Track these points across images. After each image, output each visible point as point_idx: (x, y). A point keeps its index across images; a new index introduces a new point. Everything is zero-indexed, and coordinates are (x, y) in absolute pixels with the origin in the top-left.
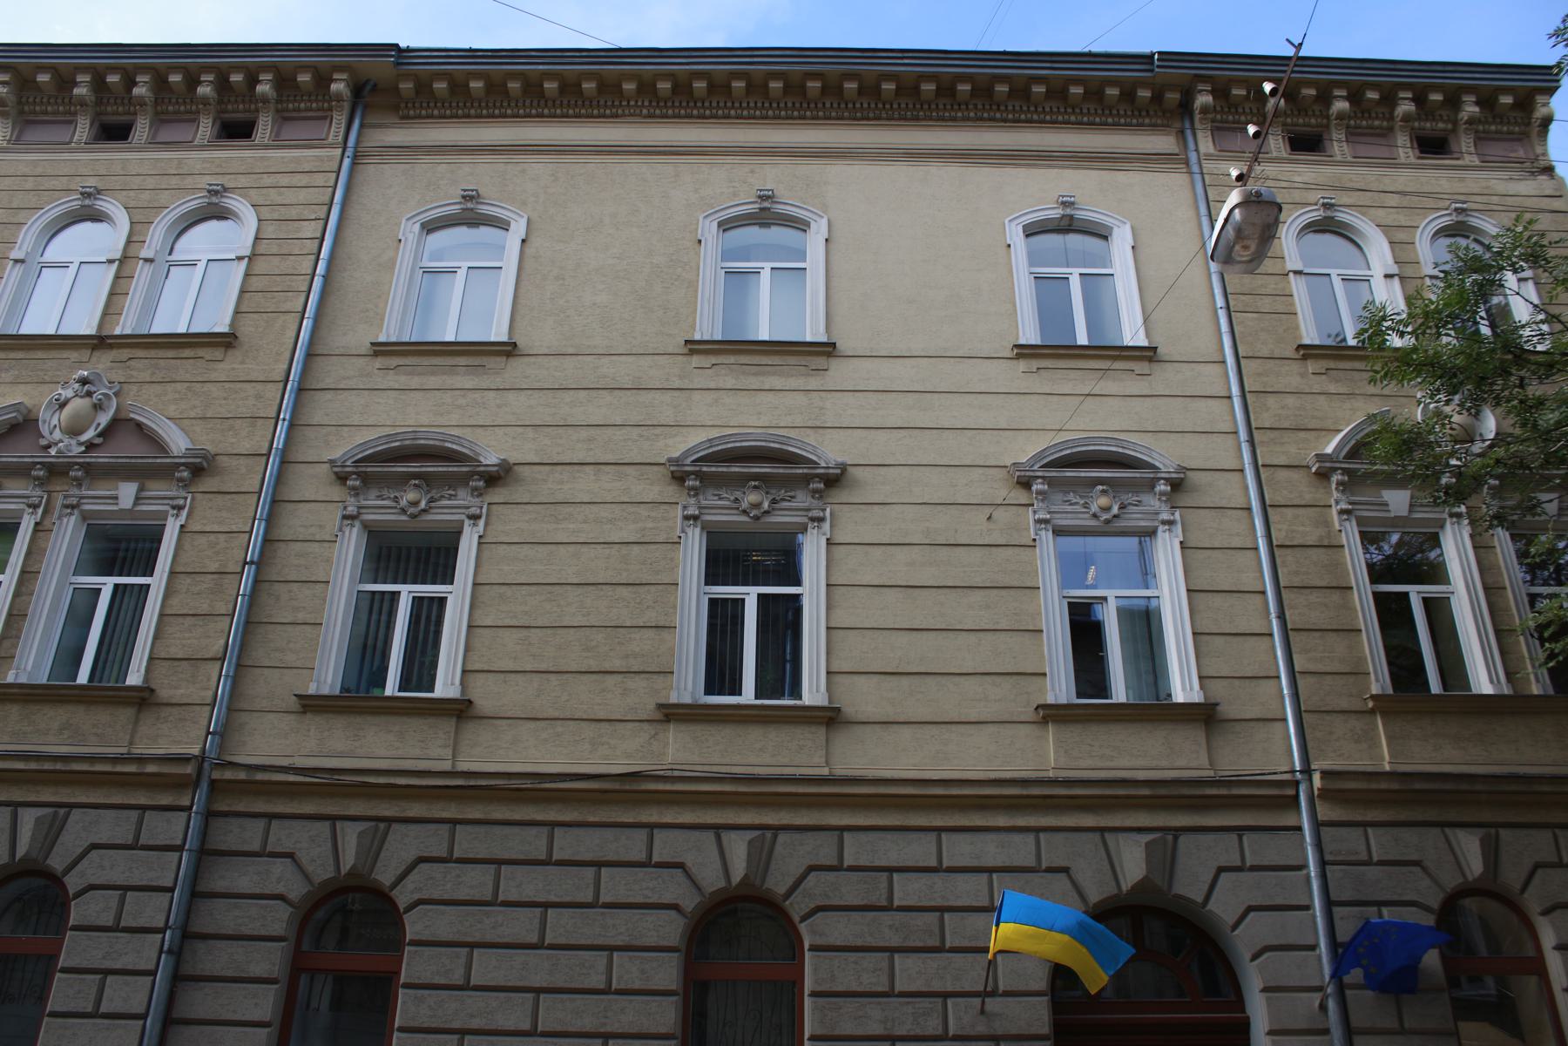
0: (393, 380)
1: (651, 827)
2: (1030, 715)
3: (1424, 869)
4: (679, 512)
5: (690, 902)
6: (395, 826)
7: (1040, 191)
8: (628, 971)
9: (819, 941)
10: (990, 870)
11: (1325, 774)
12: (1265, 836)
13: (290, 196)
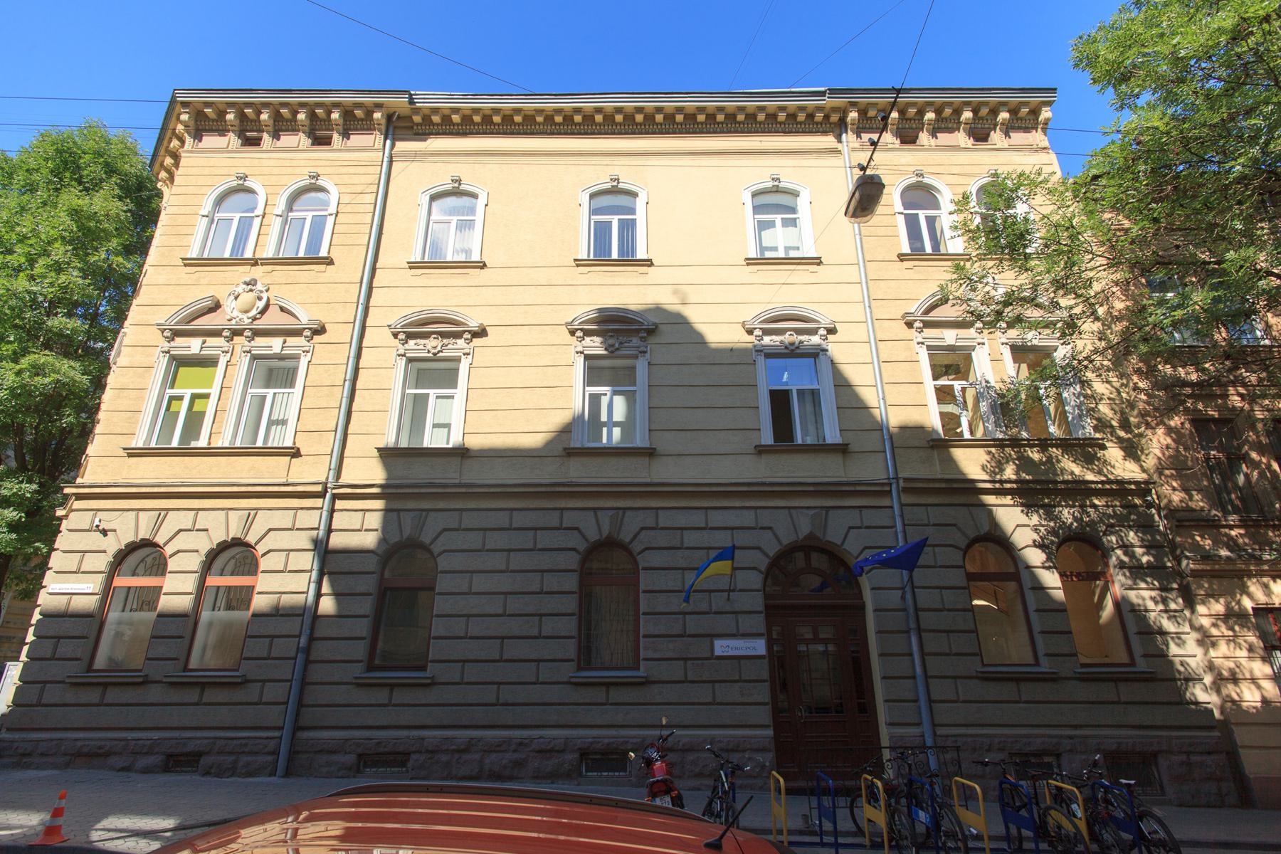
0: (419, 281)
1: (562, 509)
2: (753, 451)
3: (959, 529)
4: (573, 350)
5: (582, 546)
6: (431, 514)
7: (759, 172)
8: (552, 582)
9: (646, 565)
10: (733, 528)
11: (906, 480)
12: (873, 511)
13: (356, 179)
